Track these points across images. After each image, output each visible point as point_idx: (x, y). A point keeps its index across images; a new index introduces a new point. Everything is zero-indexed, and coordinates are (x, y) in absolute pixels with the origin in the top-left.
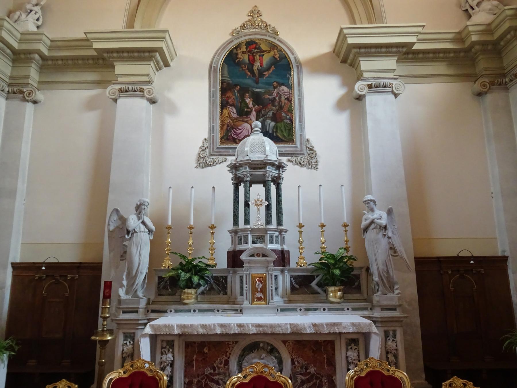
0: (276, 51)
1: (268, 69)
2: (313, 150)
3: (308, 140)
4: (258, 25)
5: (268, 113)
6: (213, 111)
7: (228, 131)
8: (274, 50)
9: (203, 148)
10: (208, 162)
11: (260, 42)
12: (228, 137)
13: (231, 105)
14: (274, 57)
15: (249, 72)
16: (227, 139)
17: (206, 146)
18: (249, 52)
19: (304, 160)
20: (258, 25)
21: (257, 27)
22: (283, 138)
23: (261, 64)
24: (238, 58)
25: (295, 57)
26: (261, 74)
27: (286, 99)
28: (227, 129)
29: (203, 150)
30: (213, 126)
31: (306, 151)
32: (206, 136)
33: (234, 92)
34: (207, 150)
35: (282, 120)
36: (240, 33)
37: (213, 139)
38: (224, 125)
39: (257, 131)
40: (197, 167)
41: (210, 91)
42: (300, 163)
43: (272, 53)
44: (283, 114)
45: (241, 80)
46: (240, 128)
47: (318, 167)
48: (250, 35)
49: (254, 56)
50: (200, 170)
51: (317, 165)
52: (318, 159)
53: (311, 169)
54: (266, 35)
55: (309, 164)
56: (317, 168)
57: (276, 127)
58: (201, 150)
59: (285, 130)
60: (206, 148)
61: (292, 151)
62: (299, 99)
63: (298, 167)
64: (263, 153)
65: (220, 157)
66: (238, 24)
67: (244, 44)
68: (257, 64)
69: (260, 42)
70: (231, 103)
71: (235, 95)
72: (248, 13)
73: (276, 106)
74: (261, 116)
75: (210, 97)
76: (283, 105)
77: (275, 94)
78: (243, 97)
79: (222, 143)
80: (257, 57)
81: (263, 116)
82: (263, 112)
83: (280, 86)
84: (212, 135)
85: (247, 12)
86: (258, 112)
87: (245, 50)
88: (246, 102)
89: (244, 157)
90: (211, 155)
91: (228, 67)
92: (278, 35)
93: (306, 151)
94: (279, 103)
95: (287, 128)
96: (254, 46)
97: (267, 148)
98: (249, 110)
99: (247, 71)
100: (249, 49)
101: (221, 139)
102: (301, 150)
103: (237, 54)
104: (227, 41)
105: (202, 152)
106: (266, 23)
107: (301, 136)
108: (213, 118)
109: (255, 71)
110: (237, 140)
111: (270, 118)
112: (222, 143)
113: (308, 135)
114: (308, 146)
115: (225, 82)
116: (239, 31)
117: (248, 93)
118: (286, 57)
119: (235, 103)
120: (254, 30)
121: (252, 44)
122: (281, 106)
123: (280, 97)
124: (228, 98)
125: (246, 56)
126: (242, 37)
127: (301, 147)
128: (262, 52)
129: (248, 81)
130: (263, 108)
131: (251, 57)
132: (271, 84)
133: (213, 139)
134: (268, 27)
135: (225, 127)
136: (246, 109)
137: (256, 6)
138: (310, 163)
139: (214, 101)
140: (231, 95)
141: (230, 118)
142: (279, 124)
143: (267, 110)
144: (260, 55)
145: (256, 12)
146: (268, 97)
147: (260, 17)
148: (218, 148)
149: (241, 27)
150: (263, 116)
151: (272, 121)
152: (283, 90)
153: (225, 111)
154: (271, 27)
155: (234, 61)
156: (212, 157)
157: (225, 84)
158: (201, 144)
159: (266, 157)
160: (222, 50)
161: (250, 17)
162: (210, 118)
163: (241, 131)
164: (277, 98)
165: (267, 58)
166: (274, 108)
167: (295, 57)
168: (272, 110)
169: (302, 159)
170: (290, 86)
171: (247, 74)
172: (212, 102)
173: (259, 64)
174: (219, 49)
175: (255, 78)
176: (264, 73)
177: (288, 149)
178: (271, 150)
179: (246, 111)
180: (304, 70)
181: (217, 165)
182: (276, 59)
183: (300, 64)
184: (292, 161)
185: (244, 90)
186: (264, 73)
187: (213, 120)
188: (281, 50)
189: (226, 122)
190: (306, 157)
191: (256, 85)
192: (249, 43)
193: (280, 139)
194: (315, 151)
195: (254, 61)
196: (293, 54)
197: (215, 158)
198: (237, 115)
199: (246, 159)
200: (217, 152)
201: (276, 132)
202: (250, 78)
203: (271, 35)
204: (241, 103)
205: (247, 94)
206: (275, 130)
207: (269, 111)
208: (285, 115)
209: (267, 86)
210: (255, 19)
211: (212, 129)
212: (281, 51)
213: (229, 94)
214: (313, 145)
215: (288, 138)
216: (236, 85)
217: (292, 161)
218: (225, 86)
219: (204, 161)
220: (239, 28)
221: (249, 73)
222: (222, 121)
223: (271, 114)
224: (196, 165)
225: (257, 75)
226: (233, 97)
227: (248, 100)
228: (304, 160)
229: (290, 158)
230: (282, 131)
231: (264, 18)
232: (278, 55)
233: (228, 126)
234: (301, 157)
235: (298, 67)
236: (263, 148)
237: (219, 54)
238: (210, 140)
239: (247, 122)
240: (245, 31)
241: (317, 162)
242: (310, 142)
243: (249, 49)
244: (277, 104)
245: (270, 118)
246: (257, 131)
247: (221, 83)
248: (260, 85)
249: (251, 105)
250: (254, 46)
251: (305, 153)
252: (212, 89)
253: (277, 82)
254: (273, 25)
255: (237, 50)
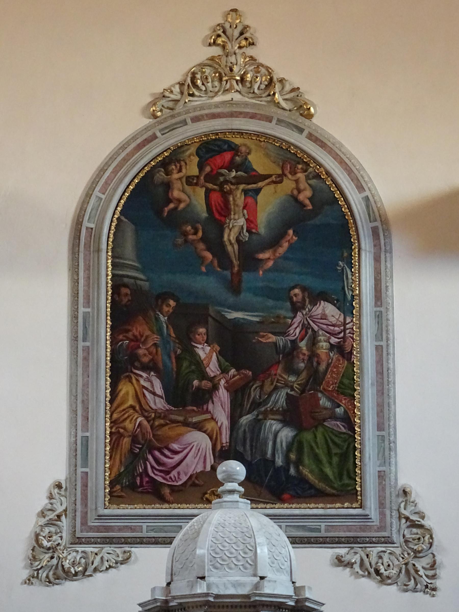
0: (301, 176)
1: (273, 242)
2: (421, 526)
3: (405, 493)
4: (242, 80)
5: (270, 395)
6: (86, 385)
7: (134, 457)
8: (293, 173)
9: (52, 516)
10: (67, 565)
11: (248, 142)
12: (134, 478)
13: (145, 368)
14: (296, 199)
15: (209, 249)
16: (133, 487)
17: (60, 509)
18: (210, 178)
19: (390, 558)
20: (242, 80)
21: (239, 87)
22: (321, 485)
23: (251, 222)
24: (169, 201)
25: (367, 199)
26: (249, 257)
27: (332, 347)
28: (131, 451)
29: (50, 523)
30: (86, 441)
31: (397, 530)
32: (61, 474)
33: (157, 319)
34: (65, 522)
35: (320, 422)
36: (180, 108)
37: (85, 486)
38: (121, 436)
39: (231, 492)
40: (28, 581)
41: (74, 316)
42: (377, 572)
43: (288, 185)
44: (324, 402)
45: (182, 280)
46: (175, 446)
47: (438, 583)
48: (214, 116)
49: (225, 195)
50: (39, 591)
51: (434, 577)
52: (438, 558)
53: (415, 590)
54: (269, 119)
55: (407, 571)
56: (434, 589)
57: (296, 445)
58: (43, 521)
59: (329, 454)
60: (59, 516)
61: (349, 529)
62: (379, 349)
63: (368, 584)
64: (250, 571)
65: (108, 548)
66: (169, 75)
67: (193, 149)
68: (238, 221)
69: (248, 142)
70: (145, 360)
71: (160, 332)
72: (207, 32)
73: (297, 373)
74: (247, 406)
75: (74, 339)
76: (323, 367)
77: (295, 331)
78: (186, 342)
79: (115, 497)
80: (238, 198)
81: (256, 405)
82: (254, 393)
83: (314, 303)
84: (80, 470)
85: (205, 30)
86: (238, 394)
87: (195, 171)
88: (194, 355)
89: (192, 585)
90: (77, 541)
91: (136, 231)
92: (309, 116)
93: (397, 530)
94: (310, 358)
95: (335, 450)
96: (228, 156)
97: (263, 552)
98: (206, 384)
99: (201, 246)
100: (208, 169)
101: (112, 484)
102: (382, 528)
103: (168, 186)
104: (134, 138)
105: (47, 530)
106: (269, 71)
107: (382, 476)
108: (86, 409)
109: (229, 248)
110: (167, 491)
111: (276, 412)
112: (115, 497)
113: (409, 471)
114: (406, 513)
115: (126, 286)
116: (177, 101)
117: (205, 324)
118: (336, 200)
119: (159, 358)
120: (227, 97)
121: (221, 152)
122: (316, 371)
123: (314, 342)
124: (137, 341)
125: (201, 192)
126: (184, 123)
127: (382, 514)
128: (252, 180)
129: (207, 284)
130: (255, 378)
131: (216, 197)
132: (280, 294)
133: (85, 486)
134: (278, 87)
135: (126, 441)
136: (196, 383)
137: (235, 10)
138: (410, 573)
139: (87, 350)
140: (148, 333)
141: (143, 410)
142: (307, 436)
143: (268, 388)
144: (245, 192)
145: (236, 33)
146: (273, 338)
147: (250, 51)
148: (100, 517)
149: (181, 85)
150: (256, 405)
151: (286, 422)
152: (324, 317)
153: (125, 388)
154: (288, 88)
155: (159, 213)
156: (80, 548)
157: (124, 291)
158: (43, 502)
159: (256, 586)
160: (115, 172)
161: (216, 51)
162: (73, 412)
163: (177, 458)
164: (303, 344)
165: (269, 203)
166: (292, 378)
167: (367, 199)
168: (287, 385)
169: (386, 558)
170: (347, 304)
171: (203, 259)
172: (80, 357)
173: (242, 222)
174: (112, 158)
175: (227, 273)
176: (261, 256)
177: (337, 523)
178: (273, 559)
179: (198, 388)
180: (398, 244)
181: (98, 575)
182: (303, 205)
183: (385, 221)
184: (350, 565)
185: (191, 315)
186: (261, 256)
187: (86, 418)
188: (318, 175)
189: (129, 425)
190: (398, 551)
191: (231, 299)
192: (213, 148)
193: (312, 486)
194: (429, 531)
195: (226, 210)
196: (360, 188)
197: (90, 549)
198: (168, 401)
199: (199, 591)
200: (98, 529)
201: (299, 462)
202: (210, 271)
203: (285, 115)
204: (178, 358)
205: (202, 330)
206: (293, 456)
207: (276, 388)
208: (328, 404)
209: (270, 303)
210: (232, 59)
211: (80, 451)
212: (318, 176)
213: (140, 328)
214: (421, 507)
215: (337, 484)
216: (163, 297)
217: (350, 565)
218: (125, 300)
219: (55, 561)
220: (177, 89)
221: (209, 256)
222: (114, 423)
223: (280, 399)
224: (25, 574)
225: (236, 263)
226: (155, 338)
227: (203, 351)
228: (390, 558)
229: (342, 551)
230: (317, 459)
231: (263, 53)
232: (308, 193)
233: (134, 440)
234: (380, 548)
235: (375, 232)
236: (251, 554)
237: (107, 183)
238: (74, 487)
239: (199, 427)
240: (197, 102)
241: (433, 566)
242: (413, 497)
243: (208, 169)
244: (302, 365)
245: (276, 412)
246: (231, 492)
247: (113, 287)
248: (246, 296)
249: (213, 368)
250: (228, 156)
251: (395, 537)
252: (82, 310)
253: (304, 289)
254: (294, 80)
255: (168, 173)
